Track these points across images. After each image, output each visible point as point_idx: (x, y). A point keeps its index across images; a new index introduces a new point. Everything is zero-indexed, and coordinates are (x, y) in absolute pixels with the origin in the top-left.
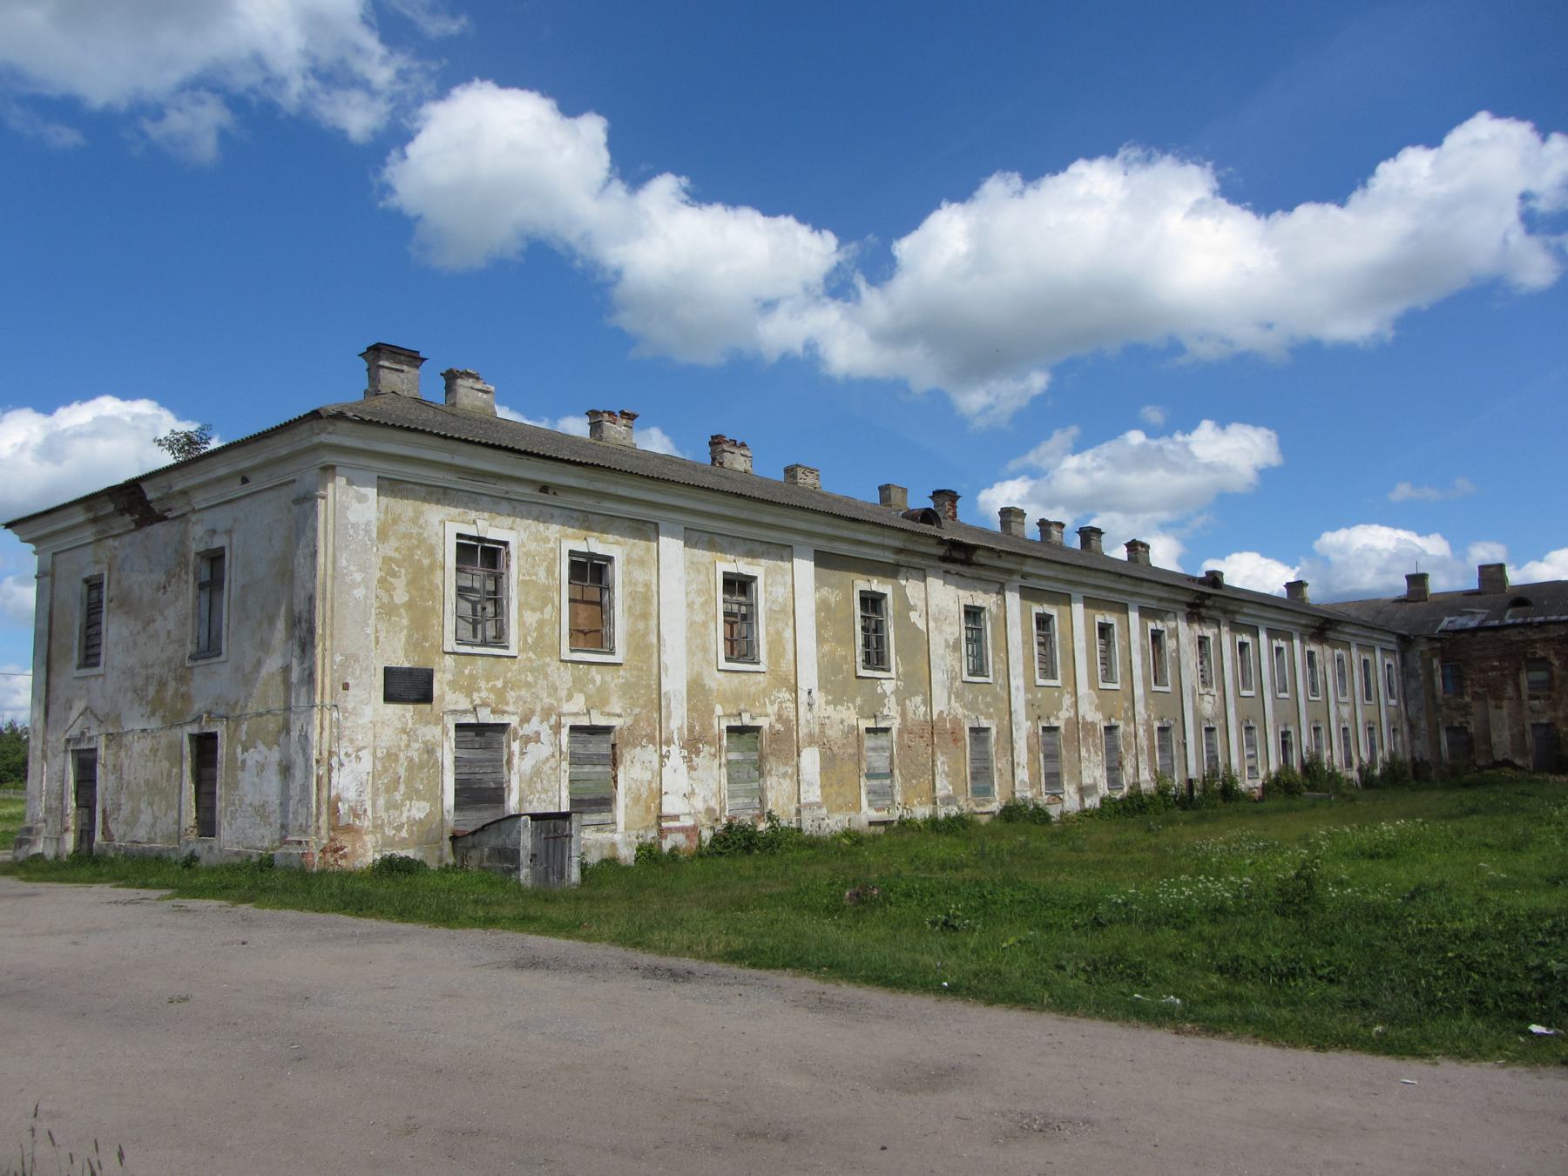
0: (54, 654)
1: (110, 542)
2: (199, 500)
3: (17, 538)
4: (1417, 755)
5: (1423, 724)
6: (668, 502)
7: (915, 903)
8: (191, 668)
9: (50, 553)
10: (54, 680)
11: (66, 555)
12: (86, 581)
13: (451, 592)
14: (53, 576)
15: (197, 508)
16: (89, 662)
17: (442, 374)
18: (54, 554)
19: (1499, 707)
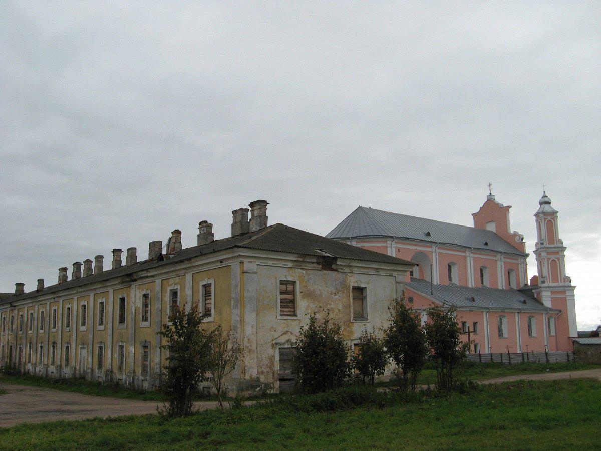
1: (300, 270)
12: (477, 323)
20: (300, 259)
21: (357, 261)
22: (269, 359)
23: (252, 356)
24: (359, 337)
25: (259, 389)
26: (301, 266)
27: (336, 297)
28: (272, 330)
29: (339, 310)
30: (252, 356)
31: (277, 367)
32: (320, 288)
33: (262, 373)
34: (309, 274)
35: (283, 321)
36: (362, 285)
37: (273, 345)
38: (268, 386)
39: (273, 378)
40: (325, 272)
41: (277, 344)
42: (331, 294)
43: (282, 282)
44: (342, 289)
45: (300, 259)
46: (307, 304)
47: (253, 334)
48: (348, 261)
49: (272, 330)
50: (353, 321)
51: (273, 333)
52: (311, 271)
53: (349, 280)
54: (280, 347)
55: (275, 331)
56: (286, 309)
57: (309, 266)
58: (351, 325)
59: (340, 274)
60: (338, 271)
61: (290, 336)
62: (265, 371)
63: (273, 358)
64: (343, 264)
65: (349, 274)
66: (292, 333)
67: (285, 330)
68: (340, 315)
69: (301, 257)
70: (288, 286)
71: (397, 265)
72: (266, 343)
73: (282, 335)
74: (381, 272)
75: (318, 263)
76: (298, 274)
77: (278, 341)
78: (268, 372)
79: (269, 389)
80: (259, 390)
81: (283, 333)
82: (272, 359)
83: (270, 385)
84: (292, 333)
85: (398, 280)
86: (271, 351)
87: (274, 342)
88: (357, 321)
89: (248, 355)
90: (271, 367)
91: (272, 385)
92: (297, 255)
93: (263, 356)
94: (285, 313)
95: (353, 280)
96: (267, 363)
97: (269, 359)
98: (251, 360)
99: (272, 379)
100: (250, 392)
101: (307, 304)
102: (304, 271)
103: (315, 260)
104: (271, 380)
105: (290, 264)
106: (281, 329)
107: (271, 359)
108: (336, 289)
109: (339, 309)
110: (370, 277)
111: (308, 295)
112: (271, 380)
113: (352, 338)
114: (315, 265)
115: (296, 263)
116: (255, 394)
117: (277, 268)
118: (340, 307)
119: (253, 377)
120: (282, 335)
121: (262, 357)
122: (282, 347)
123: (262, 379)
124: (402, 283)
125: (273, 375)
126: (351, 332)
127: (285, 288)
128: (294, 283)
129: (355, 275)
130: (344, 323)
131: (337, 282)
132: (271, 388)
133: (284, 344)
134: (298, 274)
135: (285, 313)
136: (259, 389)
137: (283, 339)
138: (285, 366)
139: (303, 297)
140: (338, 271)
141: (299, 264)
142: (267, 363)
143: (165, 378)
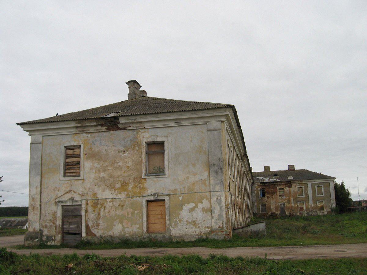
0: (43, 173)
1: (85, 135)
2: (147, 125)
3: (22, 129)
4: (254, 212)
5: (256, 204)
6: (63, 127)
7: (24, 258)
8: (145, 179)
9: (42, 135)
10: (43, 180)
11: (47, 137)
12: (65, 147)
13: (82, 156)
14: (42, 144)
15: (146, 128)
16: (66, 175)
17: (133, 84)
18: (43, 136)
19: (273, 200)
20: (79, 125)
21: (143, 116)
22: (52, 214)
23: (35, 212)
24: (153, 193)
25: (37, 240)
26: (84, 131)
27: (125, 154)
28: (56, 190)
29: (128, 167)
30: (35, 212)
31: (59, 222)
32: (107, 148)
33: (46, 226)
34: (94, 137)
35: (66, 182)
36: (159, 139)
37: (56, 203)
38: (49, 238)
39: (56, 232)
40: (112, 132)
41: (59, 202)
42: (119, 152)
43: (67, 148)
44: (133, 147)
45: (79, 125)
46: (92, 164)
47: (37, 194)
48: (133, 118)
49: (56, 190)
50: (145, 177)
51: (57, 192)
52: (97, 134)
53: (141, 137)
54: (62, 204)
55: (58, 190)
56: (72, 171)
57: (92, 129)
58: (143, 181)
59: (131, 132)
60: (126, 129)
61: (73, 195)
62: (48, 225)
63: (55, 214)
64: (128, 121)
65: (142, 131)
66: (74, 192)
67: (68, 190)
68: (129, 173)
69: (79, 123)
70: (74, 150)
71: (201, 111)
72: (49, 201)
73: (65, 194)
74: (184, 123)
75: (102, 125)
76: (83, 139)
77: (61, 199)
78: (51, 226)
79: (50, 241)
80: (38, 241)
81: (65, 192)
82: (54, 214)
83: (51, 237)
84: (74, 192)
85: (211, 127)
86: (53, 208)
87: (57, 200)
88: (151, 177)
89: (32, 212)
90: (54, 222)
91: (53, 238)
92: (74, 122)
93: (47, 212)
94: (72, 174)
95: (146, 136)
96: (51, 218)
97: (52, 214)
98: (35, 215)
99: (54, 232)
100: (29, 242)
101: (92, 164)
102: (89, 135)
103: (95, 124)
104: (53, 233)
105: (73, 131)
106: (63, 190)
107: (54, 215)
108: (125, 147)
109: (128, 167)
110: (169, 130)
111: (93, 156)
112: (53, 233)
113: (144, 195)
114: (99, 128)
115: (79, 129)
116: (33, 244)
117: (62, 136)
118: (130, 164)
119: (36, 229)
120: (65, 194)
121: (46, 213)
122: (64, 204)
123: (46, 232)
124: (216, 130)
125: (56, 229)
126: (144, 189)
127: (72, 152)
128: (79, 147)
129: (150, 130)
130: (134, 179)
131: (126, 140)
132: (53, 240)
133: (66, 202)
134: (83, 139)
135: (72, 174)
136: (37, 240)
137: (66, 197)
138: (69, 221)
139: (88, 159)
140: (126, 129)
141: (80, 129)
142: (51, 218)
143: (124, 239)
